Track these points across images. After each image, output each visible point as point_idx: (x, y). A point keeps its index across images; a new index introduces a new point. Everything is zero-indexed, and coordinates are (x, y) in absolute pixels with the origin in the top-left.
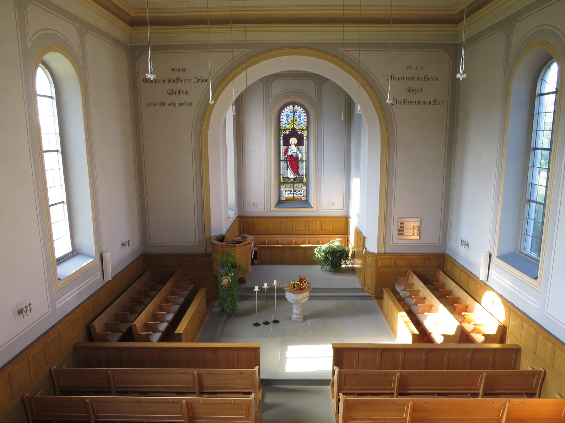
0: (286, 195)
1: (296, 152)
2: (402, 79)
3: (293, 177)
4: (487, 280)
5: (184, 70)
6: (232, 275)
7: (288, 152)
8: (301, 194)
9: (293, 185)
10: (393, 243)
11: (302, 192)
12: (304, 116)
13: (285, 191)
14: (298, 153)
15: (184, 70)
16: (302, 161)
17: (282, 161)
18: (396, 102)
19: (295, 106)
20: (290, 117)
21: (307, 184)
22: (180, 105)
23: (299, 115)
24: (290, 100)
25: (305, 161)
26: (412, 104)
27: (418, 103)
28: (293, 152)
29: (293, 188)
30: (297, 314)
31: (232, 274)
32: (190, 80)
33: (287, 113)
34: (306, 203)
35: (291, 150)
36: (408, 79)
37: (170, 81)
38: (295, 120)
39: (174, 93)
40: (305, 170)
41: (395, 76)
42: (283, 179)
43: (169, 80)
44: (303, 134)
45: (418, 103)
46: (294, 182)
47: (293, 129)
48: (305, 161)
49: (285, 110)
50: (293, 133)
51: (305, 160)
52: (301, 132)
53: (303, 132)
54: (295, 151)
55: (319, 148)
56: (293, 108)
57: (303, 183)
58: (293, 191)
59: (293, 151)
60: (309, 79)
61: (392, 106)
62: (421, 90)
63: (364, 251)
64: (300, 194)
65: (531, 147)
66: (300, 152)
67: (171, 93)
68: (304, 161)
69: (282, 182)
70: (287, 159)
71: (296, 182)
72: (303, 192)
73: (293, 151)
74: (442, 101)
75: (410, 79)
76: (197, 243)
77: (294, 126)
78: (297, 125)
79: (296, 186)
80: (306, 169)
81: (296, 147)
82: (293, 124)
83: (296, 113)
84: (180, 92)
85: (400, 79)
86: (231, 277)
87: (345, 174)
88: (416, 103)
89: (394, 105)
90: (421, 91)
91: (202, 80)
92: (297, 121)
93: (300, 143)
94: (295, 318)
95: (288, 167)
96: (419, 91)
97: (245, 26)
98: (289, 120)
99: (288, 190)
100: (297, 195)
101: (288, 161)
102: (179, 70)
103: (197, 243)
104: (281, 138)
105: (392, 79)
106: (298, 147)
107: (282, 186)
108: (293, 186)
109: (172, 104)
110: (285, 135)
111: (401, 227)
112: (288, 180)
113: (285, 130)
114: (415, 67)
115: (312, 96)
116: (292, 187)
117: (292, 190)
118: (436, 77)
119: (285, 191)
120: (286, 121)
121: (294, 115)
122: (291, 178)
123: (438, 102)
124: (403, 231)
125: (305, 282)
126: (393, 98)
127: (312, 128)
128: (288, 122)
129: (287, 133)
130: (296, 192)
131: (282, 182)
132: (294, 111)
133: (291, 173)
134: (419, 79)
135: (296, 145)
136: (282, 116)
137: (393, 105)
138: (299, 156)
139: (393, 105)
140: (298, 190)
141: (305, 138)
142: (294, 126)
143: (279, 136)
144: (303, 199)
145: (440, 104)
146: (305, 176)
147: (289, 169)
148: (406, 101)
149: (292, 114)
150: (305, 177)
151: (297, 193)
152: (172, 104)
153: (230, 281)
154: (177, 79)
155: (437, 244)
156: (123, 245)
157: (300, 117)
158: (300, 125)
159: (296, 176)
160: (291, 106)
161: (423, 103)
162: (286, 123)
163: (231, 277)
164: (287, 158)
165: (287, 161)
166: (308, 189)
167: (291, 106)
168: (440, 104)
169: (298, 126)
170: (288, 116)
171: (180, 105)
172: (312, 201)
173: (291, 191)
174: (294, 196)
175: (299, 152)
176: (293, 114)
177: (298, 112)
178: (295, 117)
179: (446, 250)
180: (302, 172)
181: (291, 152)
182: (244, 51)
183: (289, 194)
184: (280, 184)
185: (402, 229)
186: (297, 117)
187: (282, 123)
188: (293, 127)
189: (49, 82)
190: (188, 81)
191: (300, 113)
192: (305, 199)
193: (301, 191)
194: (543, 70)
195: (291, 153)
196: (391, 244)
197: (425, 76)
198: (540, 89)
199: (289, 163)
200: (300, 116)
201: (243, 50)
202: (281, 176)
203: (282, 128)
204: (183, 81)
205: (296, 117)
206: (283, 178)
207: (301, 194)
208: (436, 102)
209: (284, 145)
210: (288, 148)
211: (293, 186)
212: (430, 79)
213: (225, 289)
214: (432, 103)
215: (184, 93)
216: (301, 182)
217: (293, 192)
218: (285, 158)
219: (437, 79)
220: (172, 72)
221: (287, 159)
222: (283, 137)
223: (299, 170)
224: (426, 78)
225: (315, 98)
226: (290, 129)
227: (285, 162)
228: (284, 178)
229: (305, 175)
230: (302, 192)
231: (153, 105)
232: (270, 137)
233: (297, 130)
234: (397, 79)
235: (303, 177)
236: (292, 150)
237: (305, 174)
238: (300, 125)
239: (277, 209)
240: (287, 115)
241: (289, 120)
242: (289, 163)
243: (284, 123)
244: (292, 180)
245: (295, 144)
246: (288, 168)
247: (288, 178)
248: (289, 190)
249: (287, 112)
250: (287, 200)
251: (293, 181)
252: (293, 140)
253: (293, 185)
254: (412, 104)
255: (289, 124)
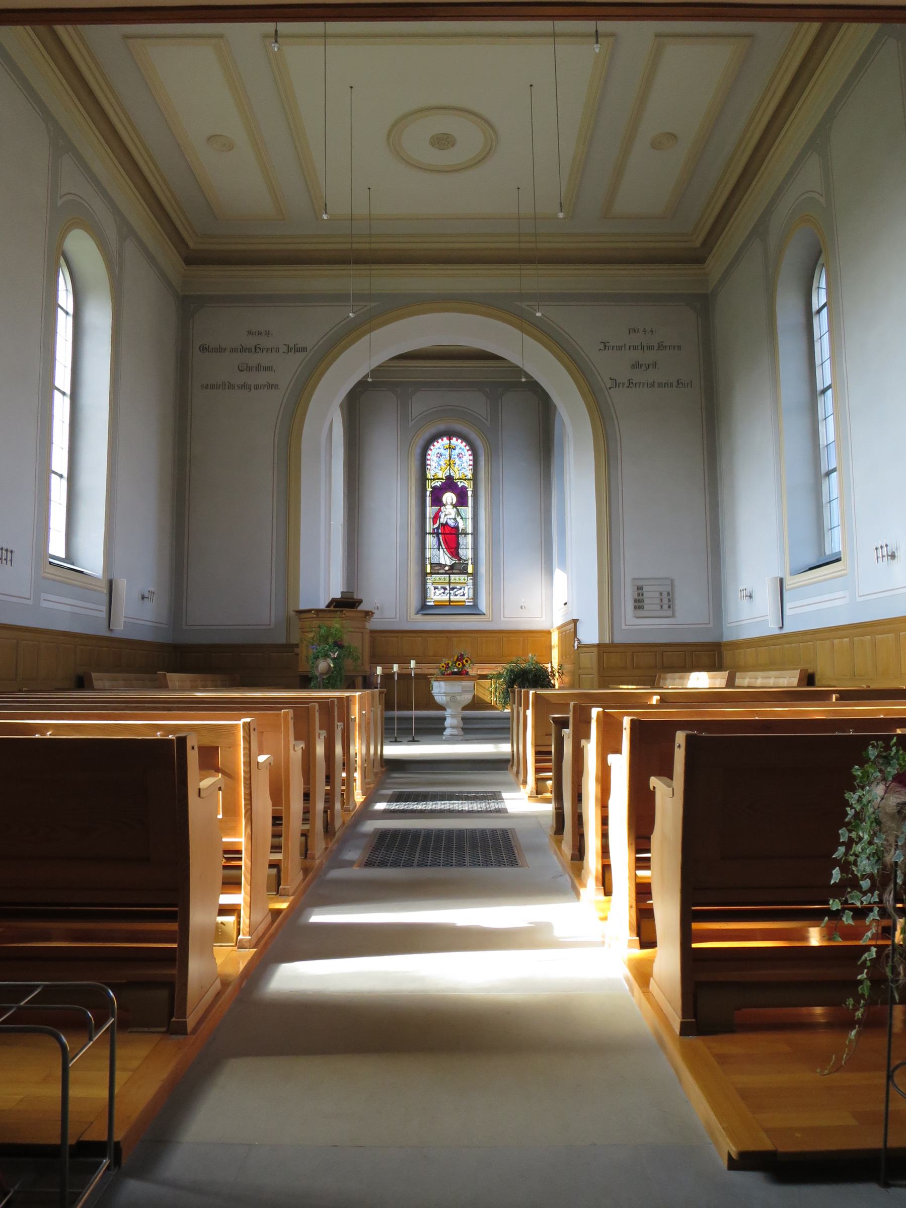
0: (436, 596)
1: (453, 517)
2: (623, 349)
3: (448, 563)
4: (781, 626)
5: (268, 333)
6: (336, 656)
7: (440, 518)
8: (464, 595)
9: (450, 577)
10: (626, 625)
11: (466, 591)
12: (468, 457)
13: (435, 588)
14: (459, 519)
15: (268, 333)
16: (466, 534)
17: (429, 533)
18: (616, 384)
19: (452, 439)
20: (443, 457)
21: (475, 575)
22: (257, 387)
23: (459, 454)
24: (442, 426)
25: (471, 534)
26: (641, 386)
27: (652, 385)
28: (450, 519)
29: (450, 583)
30: (452, 727)
31: (336, 654)
32: (277, 349)
33: (438, 451)
34: (473, 609)
35: (446, 515)
36: (631, 348)
37: (243, 350)
38: (451, 463)
39: (248, 370)
40: (470, 550)
41: (611, 344)
42: (431, 567)
43: (243, 348)
44: (467, 486)
45: (652, 385)
46: (451, 572)
47: (450, 478)
48: (471, 534)
49: (434, 446)
50: (450, 484)
51: (470, 532)
52: (462, 484)
53: (466, 484)
54: (453, 516)
55: (493, 505)
56: (449, 442)
57: (467, 573)
58: (448, 589)
59: (449, 517)
60: (476, 389)
61: (609, 391)
62: (655, 365)
63: (576, 644)
64: (462, 594)
65: (818, 389)
66: (462, 518)
67: (245, 368)
68: (468, 534)
69: (428, 571)
70: (438, 530)
71: (454, 571)
72: (468, 591)
73: (449, 517)
74: (691, 382)
75: (635, 348)
76: (272, 626)
77: (450, 473)
78: (456, 469)
79: (455, 579)
80: (472, 549)
81: (455, 509)
82: (450, 469)
83: (454, 451)
84: (259, 368)
85: (620, 348)
86: (334, 659)
87: (543, 556)
88: (649, 385)
89: (611, 389)
90: (654, 366)
91: (296, 349)
92: (455, 464)
93: (462, 501)
94: (449, 734)
95: (440, 544)
96: (651, 366)
97: (369, 268)
98: (442, 463)
99: (439, 587)
100: (456, 595)
101: (440, 534)
102: (260, 333)
103: (272, 626)
104: (428, 493)
105: (607, 348)
106: (458, 510)
107: (430, 580)
108: (450, 579)
109: (244, 386)
110: (434, 489)
111: (638, 595)
112: (440, 569)
113: (434, 479)
114: (641, 330)
115: (480, 417)
116: (448, 582)
117: (448, 587)
118: (677, 345)
119: (435, 588)
120: (437, 464)
121: (450, 453)
122: (446, 565)
123: (685, 383)
124: (642, 601)
125: (467, 661)
126: (610, 379)
127: (482, 474)
128: (439, 465)
129: (438, 484)
130: (455, 590)
131: (428, 571)
132: (450, 448)
133: (445, 555)
134: (650, 348)
135: (455, 506)
136: (429, 455)
137: (610, 388)
138: (459, 526)
139: (610, 388)
140: (458, 587)
141: (470, 494)
142: (451, 472)
143: (424, 490)
144: (467, 604)
145: (688, 387)
146: (470, 561)
147: (442, 548)
148: (632, 383)
149: (447, 453)
150: (472, 563)
151: (457, 593)
152: (244, 386)
153: (332, 665)
154: (256, 348)
155: (705, 626)
156: (143, 598)
157: (460, 458)
158: (461, 470)
159: (454, 562)
160: (445, 439)
161: (660, 385)
162: (437, 467)
163: (334, 659)
164: (438, 528)
165: (438, 534)
166: (477, 585)
167: (445, 439)
168: (688, 387)
169: (457, 473)
170: (440, 455)
171: (257, 387)
172: (483, 606)
173: (445, 589)
174: (452, 597)
175: (460, 517)
176: (449, 452)
177: (457, 448)
178: (452, 456)
179: (722, 635)
180: (466, 552)
181: (446, 517)
182: (365, 306)
183: (442, 594)
184: (424, 575)
185: (641, 597)
186: (456, 457)
187: (429, 467)
188: (448, 474)
189: (65, 289)
190: (274, 351)
191: (460, 451)
192: (471, 604)
193: (464, 588)
194: (816, 272)
195: (445, 520)
196: (623, 627)
197: (659, 344)
198: (817, 303)
199: (441, 538)
200: (460, 456)
201: (365, 304)
202: (428, 562)
203: (429, 476)
204: (265, 351)
205: (455, 457)
206: (431, 564)
207: (464, 595)
208: (682, 383)
209: (432, 505)
210: (440, 510)
211: (450, 579)
212: (668, 348)
213: (321, 682)
214: (675, 384)
215: (265, 369)
216: (464, 572)
217: (450, 590)
218: (434, 529)
219: (679, 348)
220: (247, 335)
221: (438, 530)
222: (431, 492)
223: (460, 550)
224: (661, 347)
225: (486, 422)
226: (444, 478)
227: (434, 535)
228: (433, 565)
229: (470, 560)
230: (466, 591)
231: (212, 387)
232: (408, 492)
233: (456, 479)
234: (615, 348)
235: (467, 562)
236: (447, 515)
237: (470, 557)
238: (461, 470)
239: (419, 616)
240: (438, 453)
241: (442, 463)
242: (441, 538)
243: (433, 468)
244: (447, 568)
245: (452, 504)
246: (441, 547)
247: (440, 565)
248: (442, 588)
249: (439, 448)
250: (438, 606)
251: (449, 570)
252: (449, 497)
253: (450, 577)
254: (641, 386)
255: (441, 470)
